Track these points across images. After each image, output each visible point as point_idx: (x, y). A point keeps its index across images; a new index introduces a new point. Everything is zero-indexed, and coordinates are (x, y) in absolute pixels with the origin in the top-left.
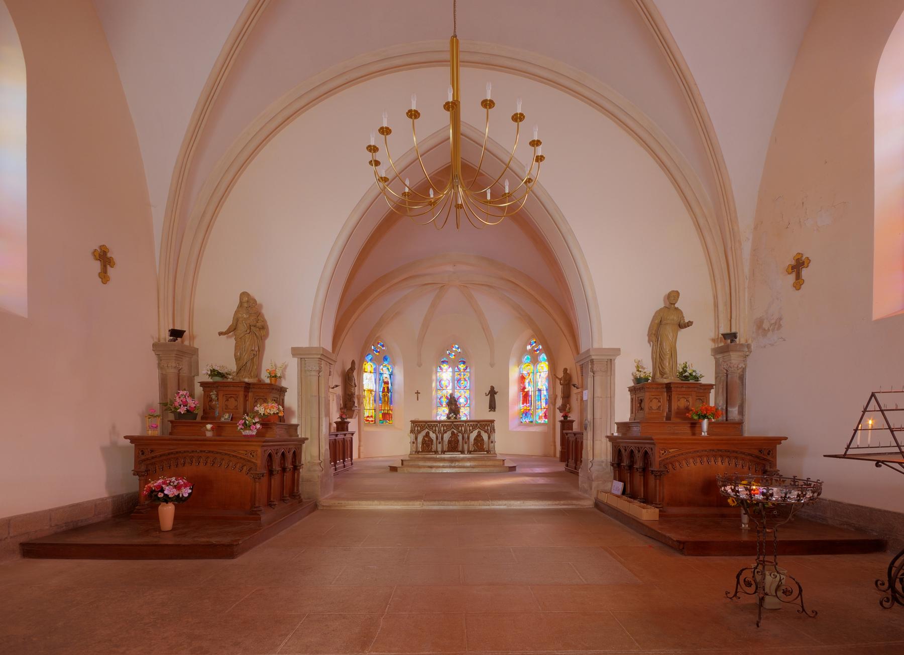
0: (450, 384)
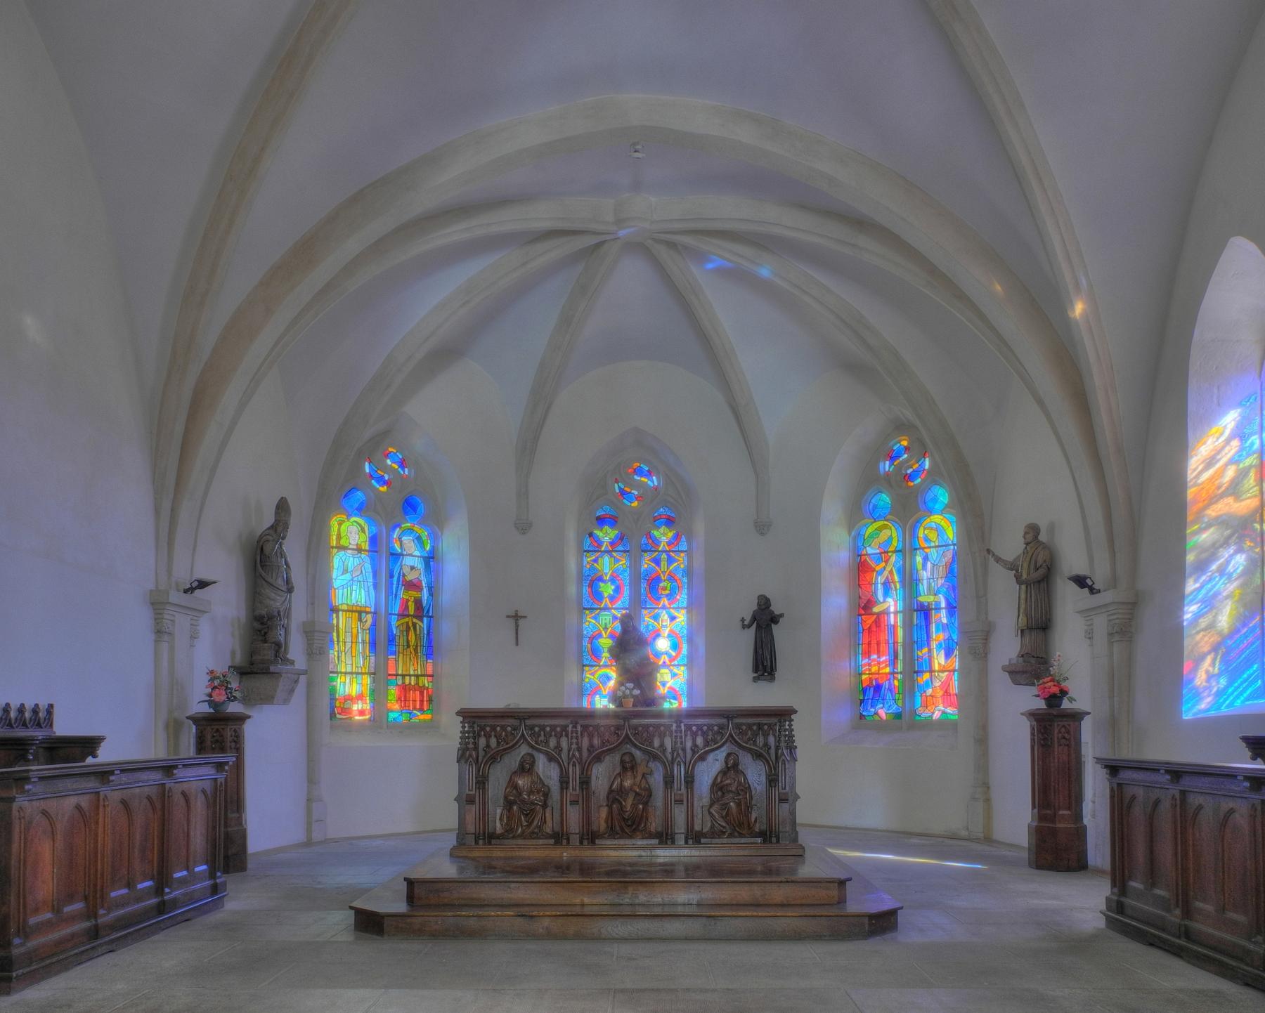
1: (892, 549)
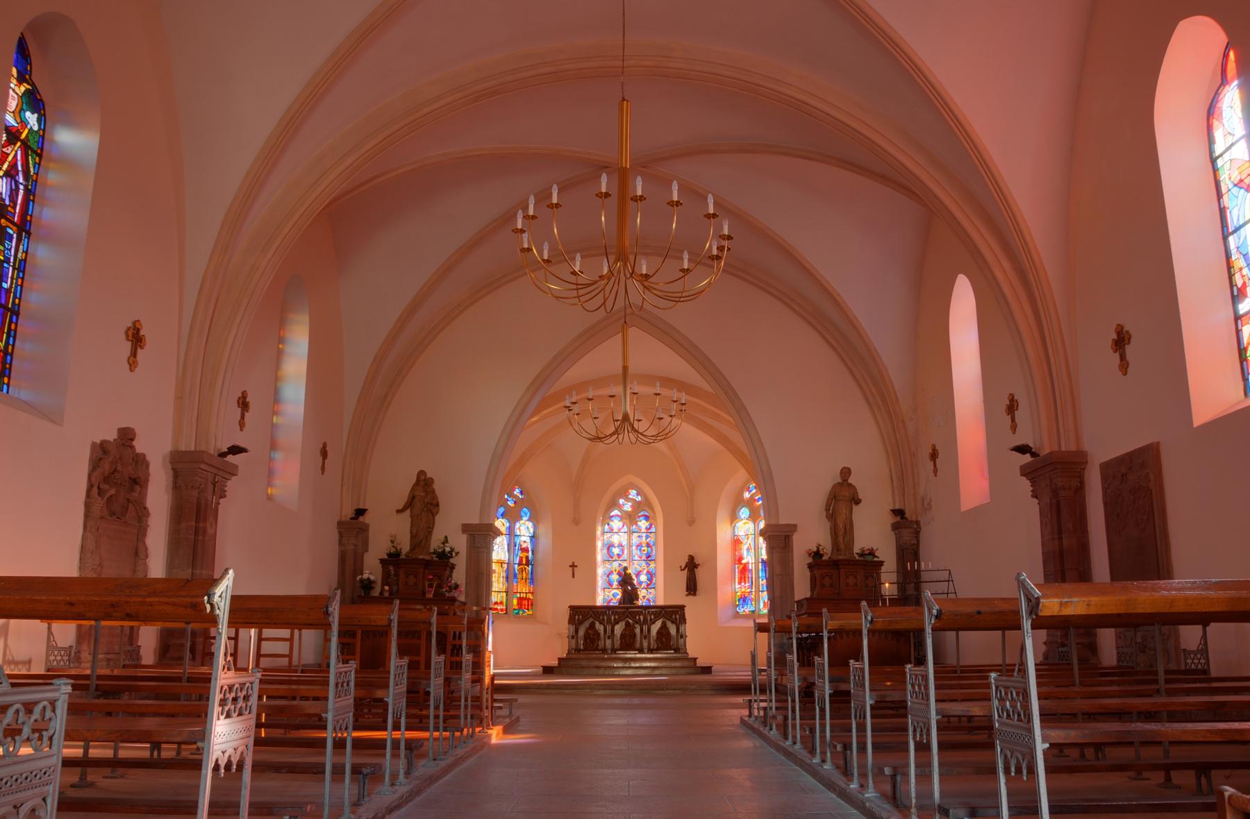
0: (624, 551)
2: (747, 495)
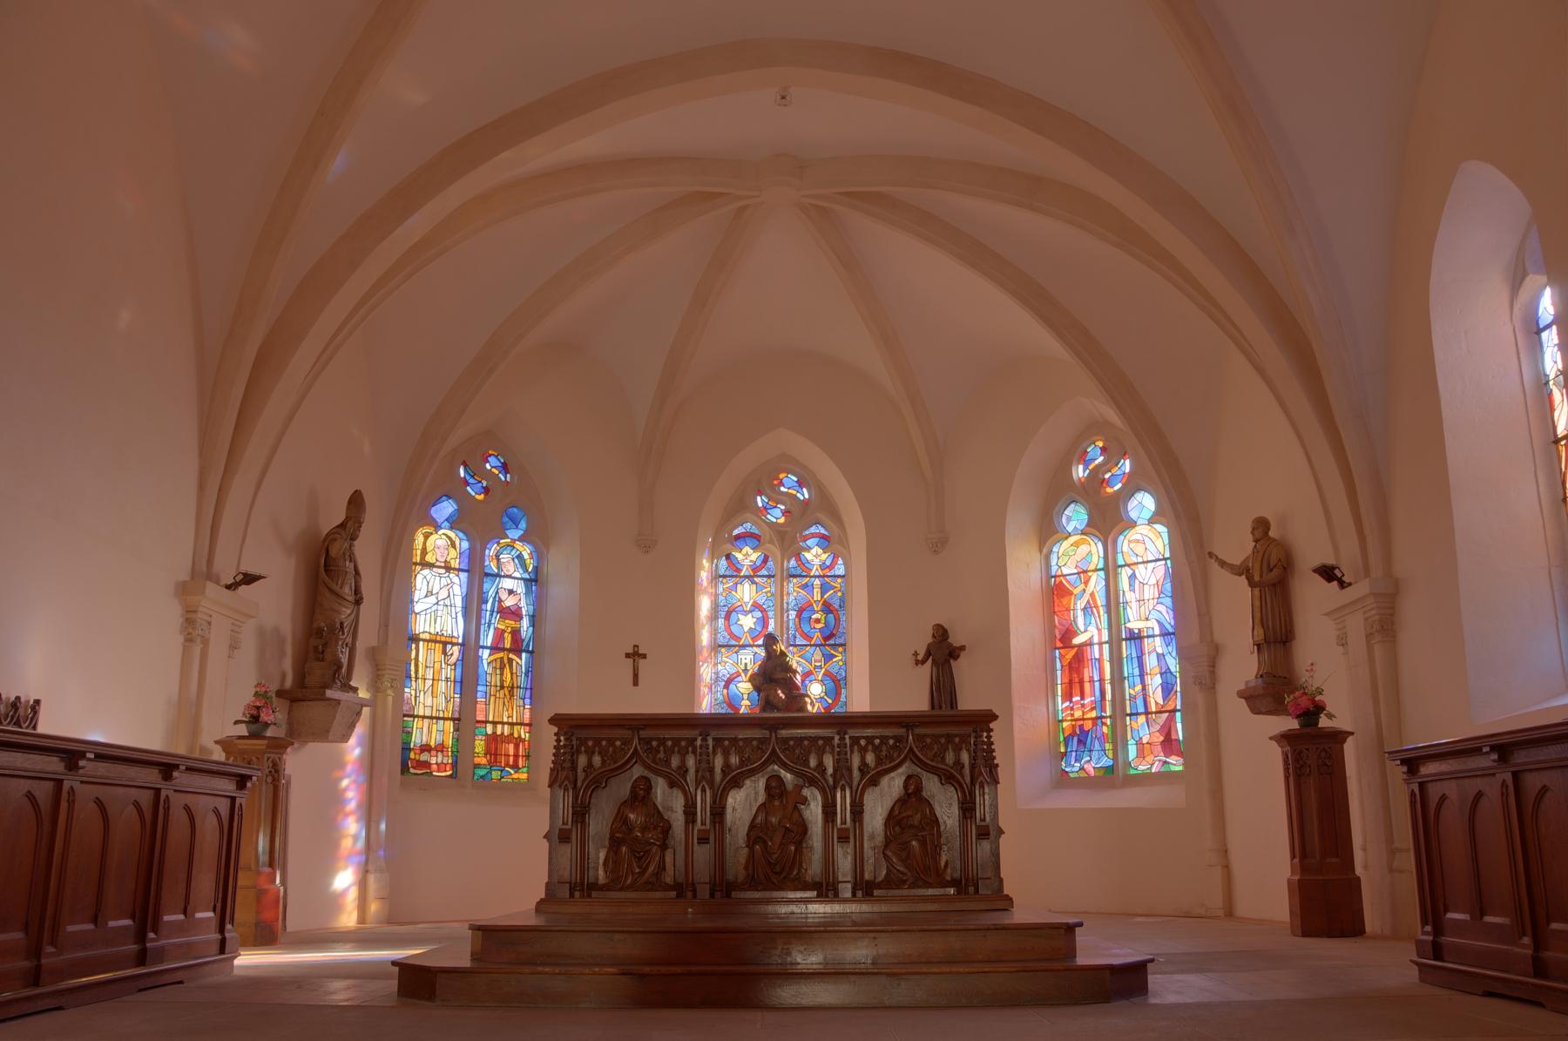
1: (1092, 567)
2: (1080, 472)
